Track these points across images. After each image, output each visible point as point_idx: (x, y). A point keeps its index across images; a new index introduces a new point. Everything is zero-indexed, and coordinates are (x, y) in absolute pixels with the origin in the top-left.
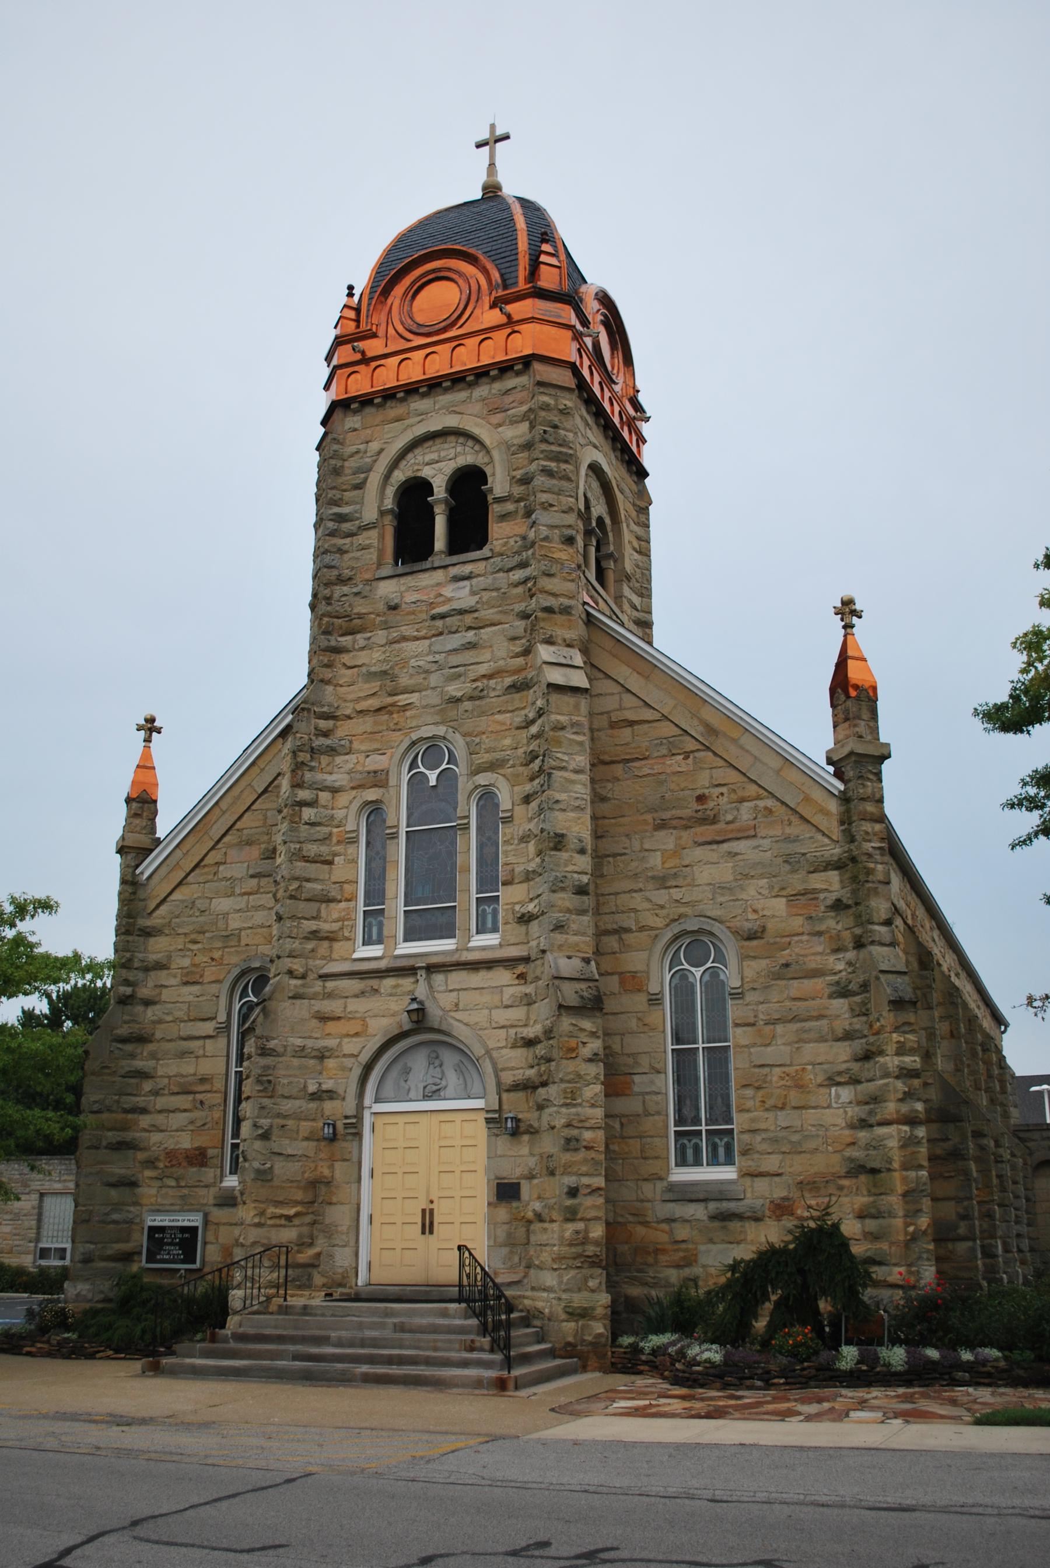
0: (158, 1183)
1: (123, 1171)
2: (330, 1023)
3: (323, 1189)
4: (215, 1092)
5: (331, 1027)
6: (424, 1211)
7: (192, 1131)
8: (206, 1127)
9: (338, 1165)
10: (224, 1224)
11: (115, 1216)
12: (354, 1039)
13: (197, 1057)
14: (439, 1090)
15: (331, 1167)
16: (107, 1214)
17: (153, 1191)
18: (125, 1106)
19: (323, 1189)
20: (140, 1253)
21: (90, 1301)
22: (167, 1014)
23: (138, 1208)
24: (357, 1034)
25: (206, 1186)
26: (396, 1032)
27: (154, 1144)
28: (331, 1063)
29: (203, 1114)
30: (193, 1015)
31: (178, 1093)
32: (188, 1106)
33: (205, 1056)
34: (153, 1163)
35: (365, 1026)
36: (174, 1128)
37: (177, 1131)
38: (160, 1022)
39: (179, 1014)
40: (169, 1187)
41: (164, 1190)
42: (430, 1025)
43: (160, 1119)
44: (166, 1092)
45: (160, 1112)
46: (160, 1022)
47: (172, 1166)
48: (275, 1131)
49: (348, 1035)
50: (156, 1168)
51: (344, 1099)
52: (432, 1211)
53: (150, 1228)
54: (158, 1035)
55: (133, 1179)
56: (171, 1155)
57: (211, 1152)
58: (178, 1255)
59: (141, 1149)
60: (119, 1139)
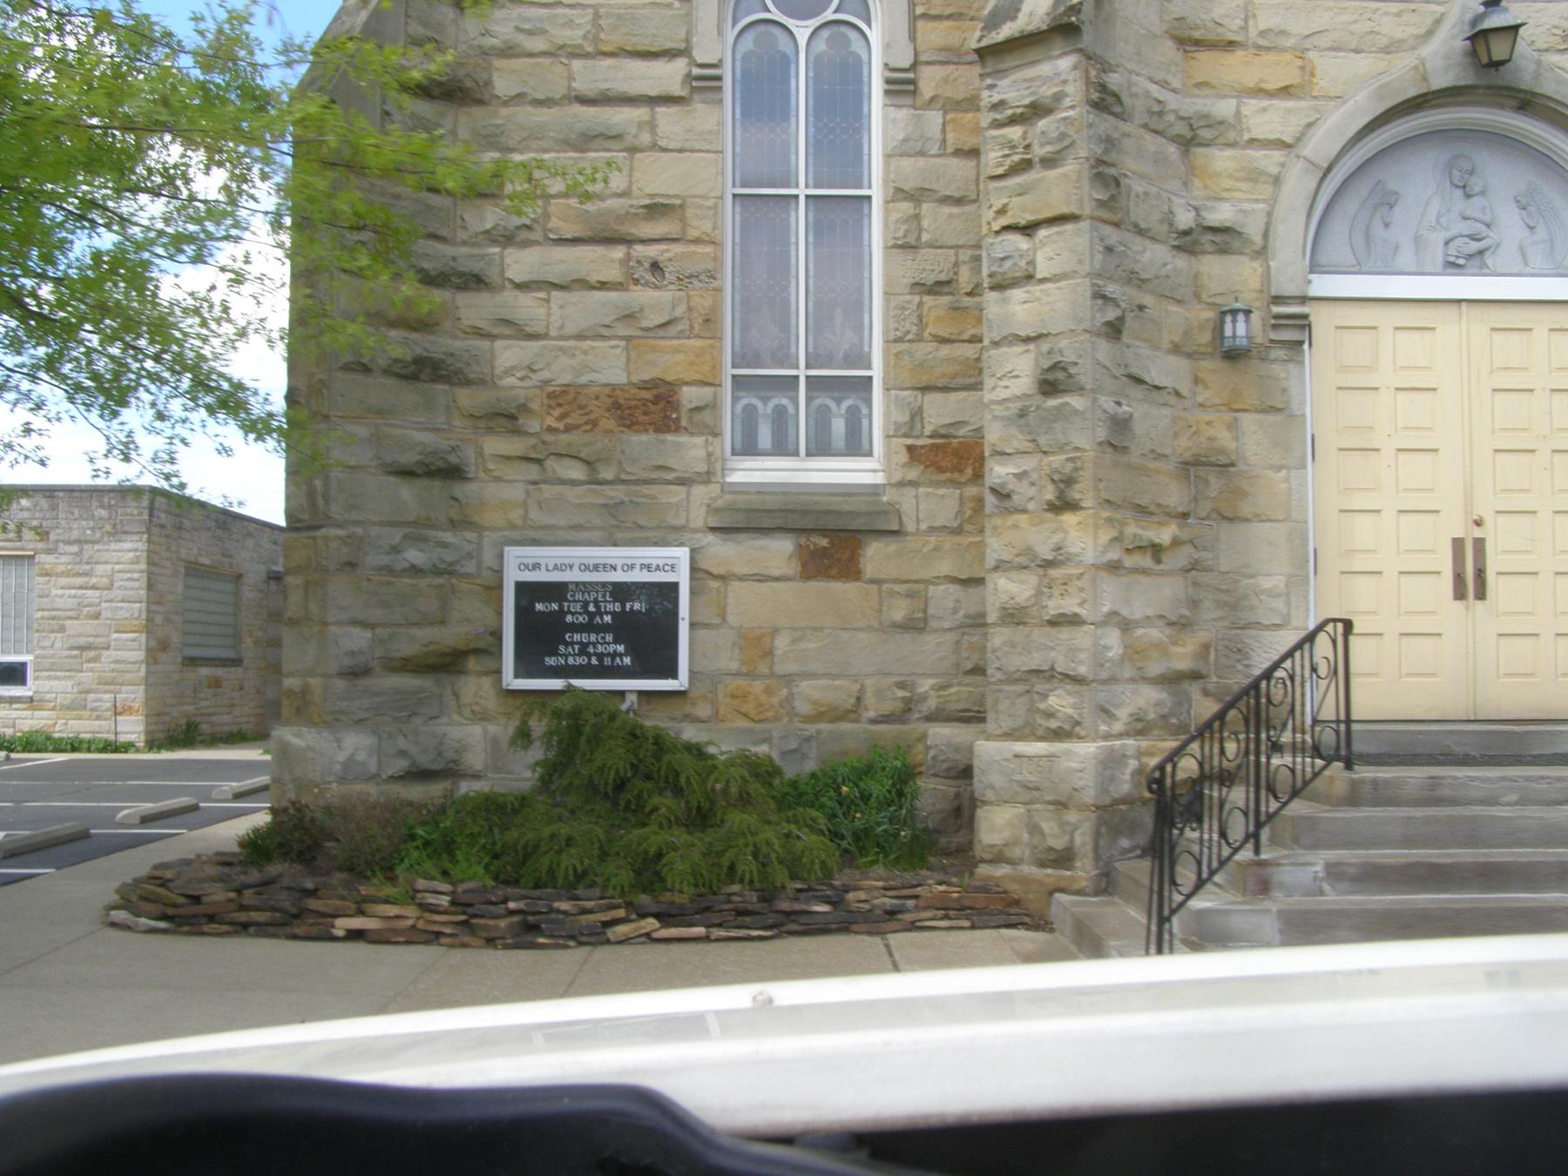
0: (533, 471)
1: (426, 438)
2: (1204, 56)
3: (1215, 483)
4: (697, 241)
5: (1207, 64)
6: (1458, 544)
7: (628, 339)
8: (672, 330)
9: (1248, 421)
10: (741, 578)
11: (414, 556)
12: (1276, 102)
13: (633, 150)
14: (1481, 252)
15: (1233, 426)
16: (396, 550)
17: (516, 492)
18: (425, 265)
19: (1215, 483)
20: (495, 651)
21: (373, 778)
22: (530, 33)
23: (469, 535)
24: (1286, 91)
25: (681, 482)
26: (1412, 92)
27: (508, 372)
28: (1222, 160)
29: (665, 296)
30: (611, 40)
31: (575, 241)
32: (613, 274)
33: (654, 147)
34: (512, 417)
35: (1308, 71)
36: (570, 329)
37: (580, 337)
38: (509, 51)
39: (572, 36)
40: (563, 482)
41: (549, 491)
42: (1526, 81)
43: (527, 307)
44: (537, 235)
45: (522, 287)
46: (509, 51)
47: (568, 429)
48: (1130, 323)
49: (1259, 92)
50: (518, 432)
51: (1262, 253)
52: (1479, 545)
53: (521, 588)
54: (503, 85)
55: (453, 459)
56: (564, 398)
57: (690, 396)
58: (614, 655)
59: (468, 383)
60: (419, 351)
